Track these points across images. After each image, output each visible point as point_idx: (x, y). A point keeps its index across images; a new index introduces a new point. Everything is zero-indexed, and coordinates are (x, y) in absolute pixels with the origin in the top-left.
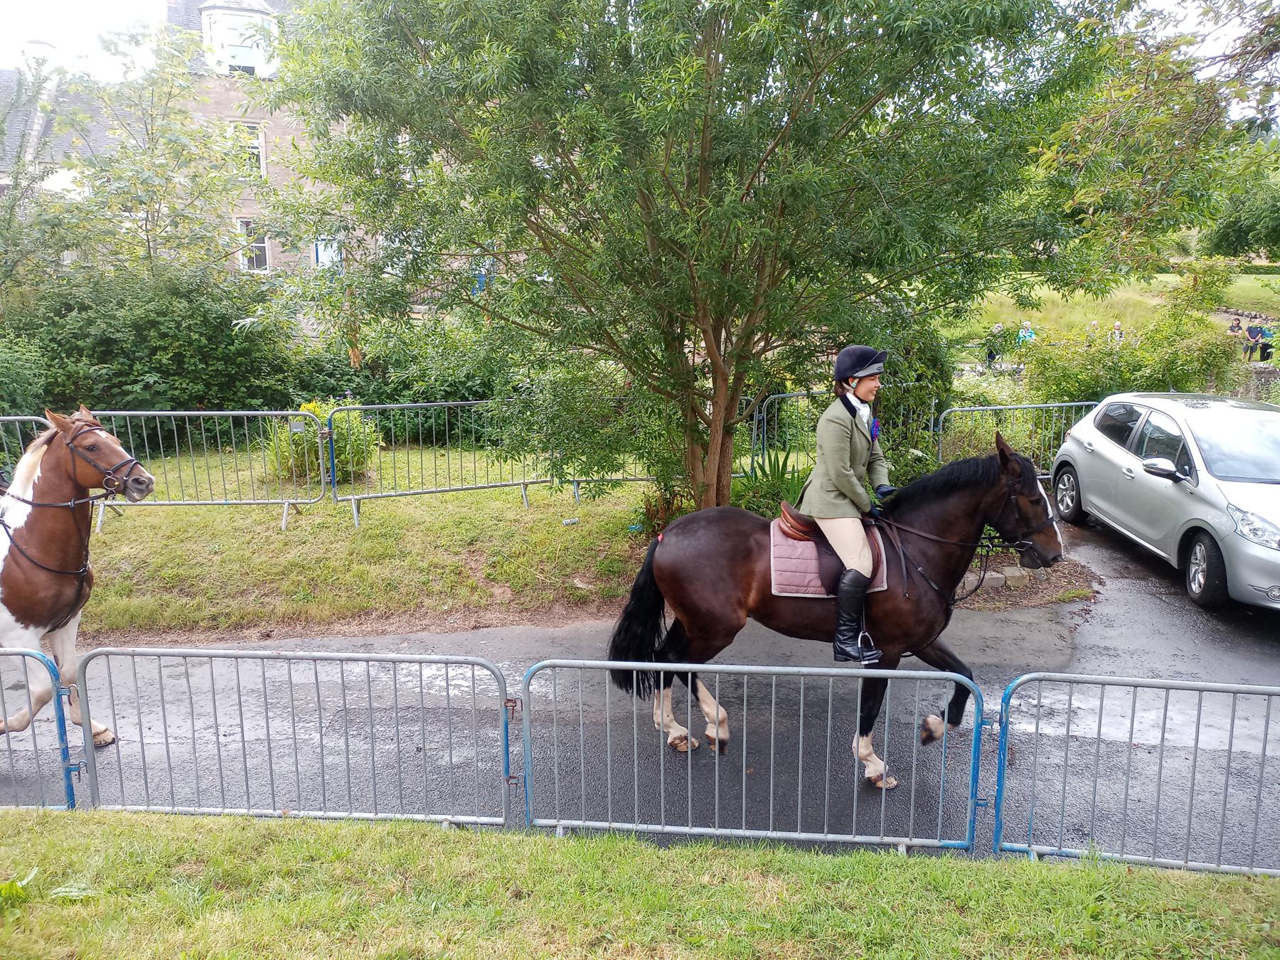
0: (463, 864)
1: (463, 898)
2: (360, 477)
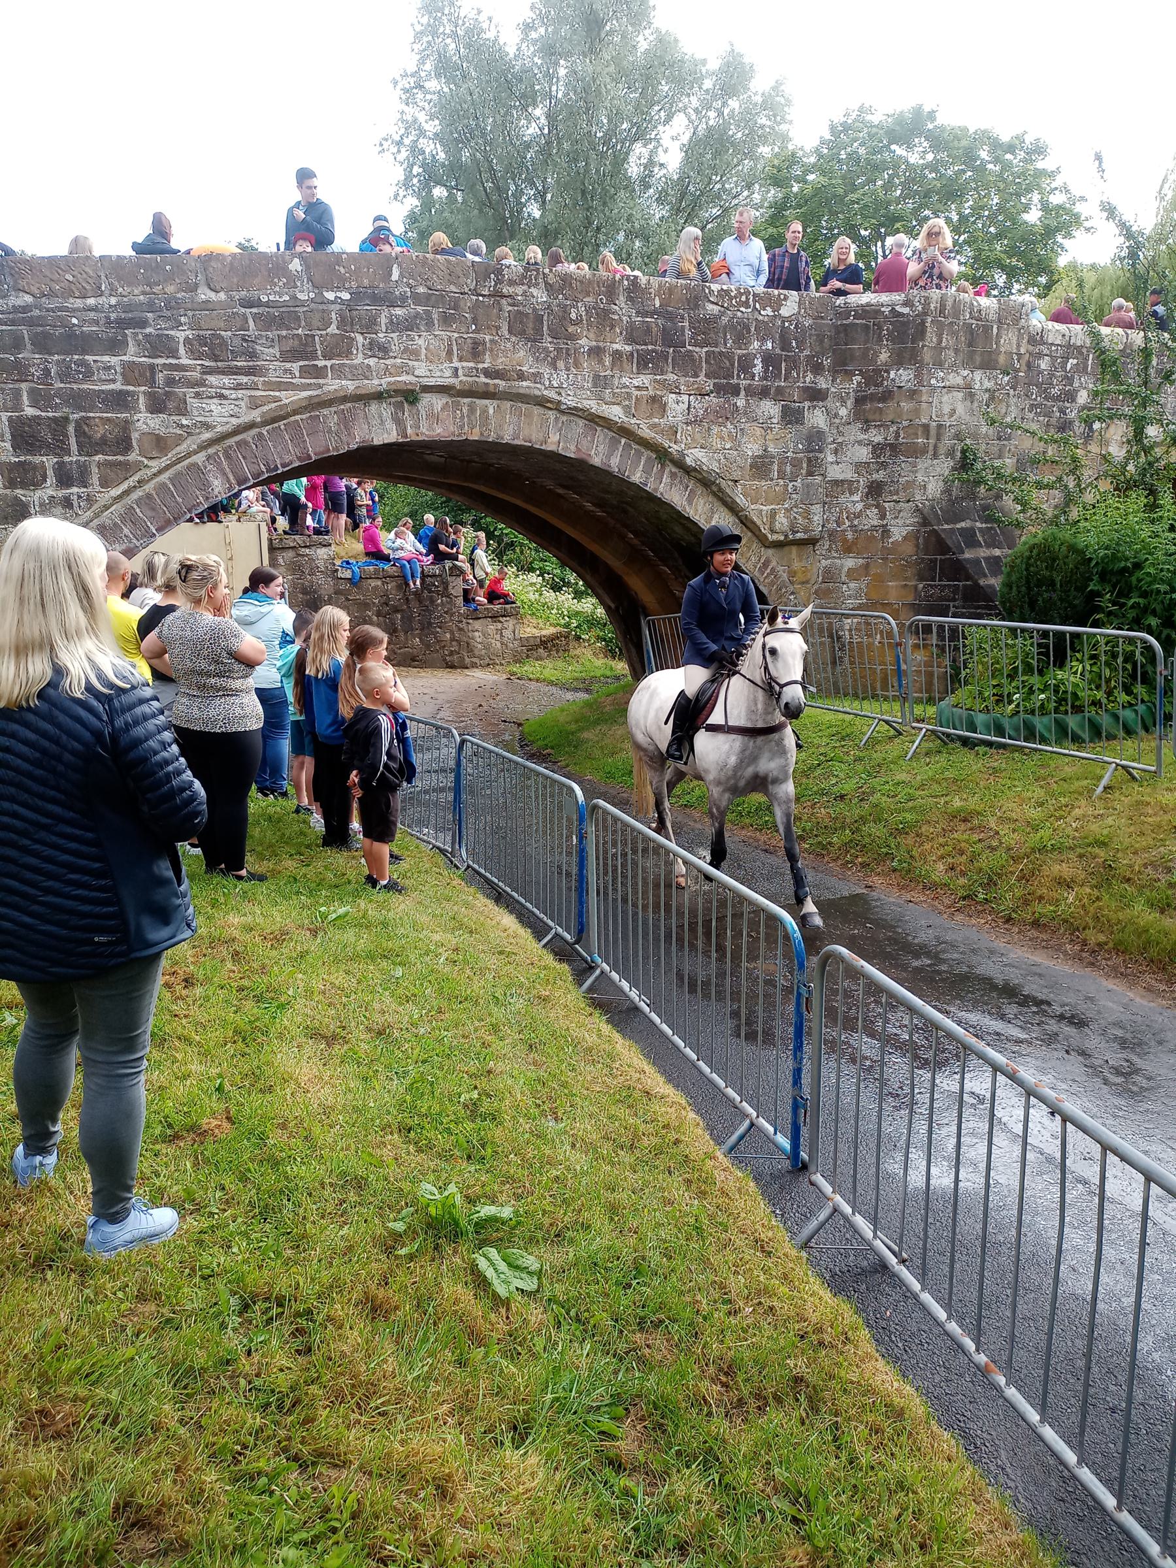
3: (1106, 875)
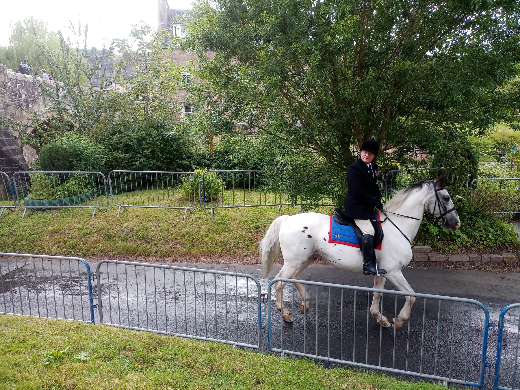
0: (237, 364)
1: (234, 380)
2: (215, 200)
3: (108, 237)
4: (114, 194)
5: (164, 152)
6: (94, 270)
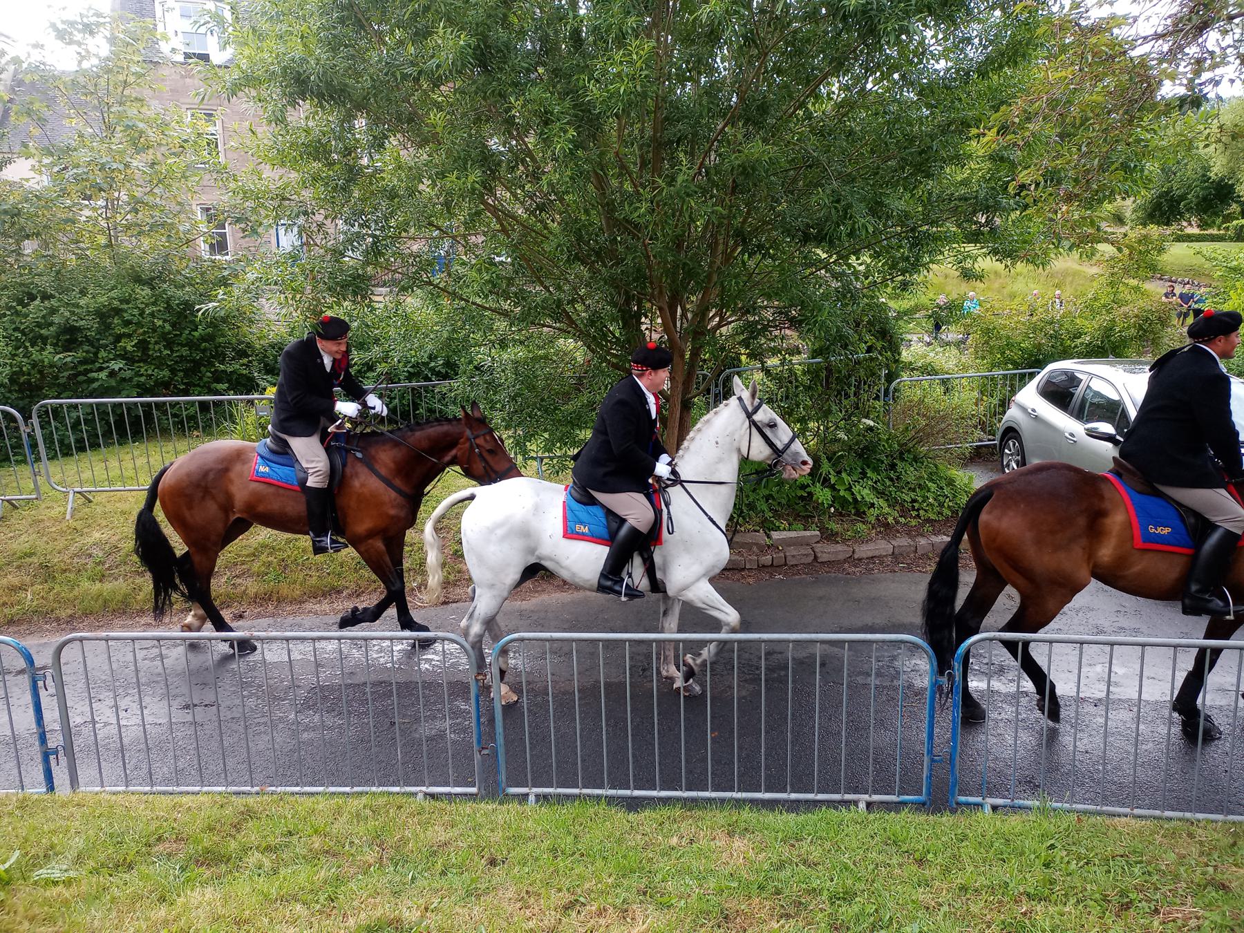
0: (438, 834)
1: (439, 867)
3: (47, 572)
4: (52, 458)
5: (173, 342)
6: (43, 659)
